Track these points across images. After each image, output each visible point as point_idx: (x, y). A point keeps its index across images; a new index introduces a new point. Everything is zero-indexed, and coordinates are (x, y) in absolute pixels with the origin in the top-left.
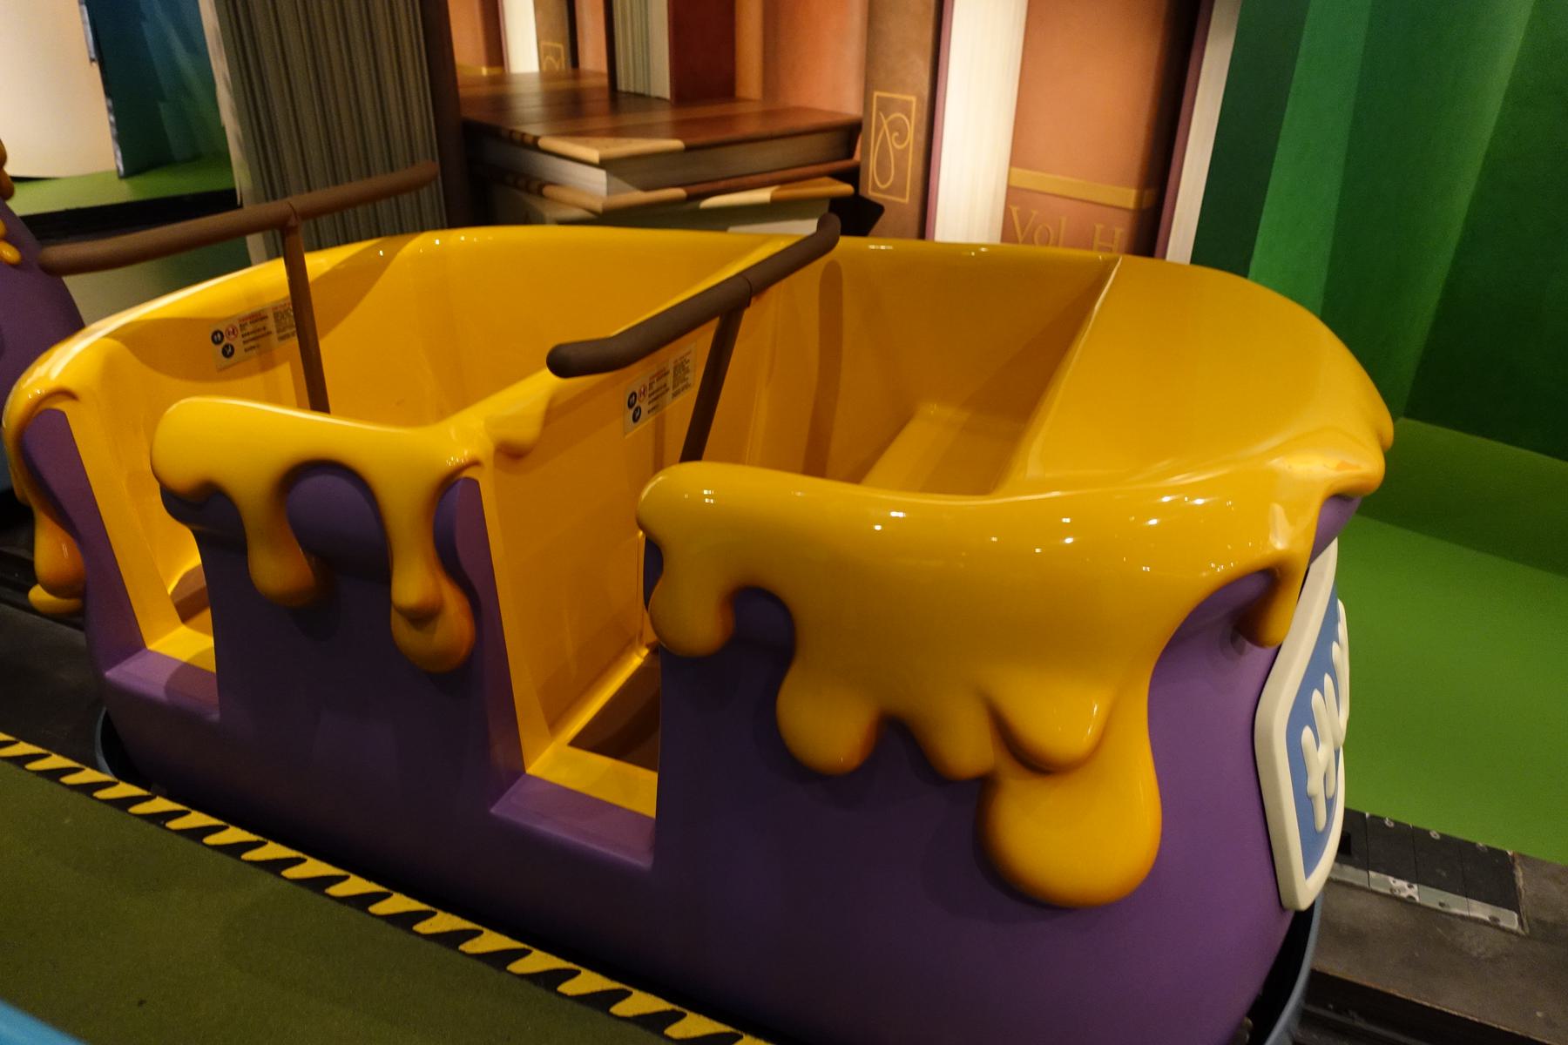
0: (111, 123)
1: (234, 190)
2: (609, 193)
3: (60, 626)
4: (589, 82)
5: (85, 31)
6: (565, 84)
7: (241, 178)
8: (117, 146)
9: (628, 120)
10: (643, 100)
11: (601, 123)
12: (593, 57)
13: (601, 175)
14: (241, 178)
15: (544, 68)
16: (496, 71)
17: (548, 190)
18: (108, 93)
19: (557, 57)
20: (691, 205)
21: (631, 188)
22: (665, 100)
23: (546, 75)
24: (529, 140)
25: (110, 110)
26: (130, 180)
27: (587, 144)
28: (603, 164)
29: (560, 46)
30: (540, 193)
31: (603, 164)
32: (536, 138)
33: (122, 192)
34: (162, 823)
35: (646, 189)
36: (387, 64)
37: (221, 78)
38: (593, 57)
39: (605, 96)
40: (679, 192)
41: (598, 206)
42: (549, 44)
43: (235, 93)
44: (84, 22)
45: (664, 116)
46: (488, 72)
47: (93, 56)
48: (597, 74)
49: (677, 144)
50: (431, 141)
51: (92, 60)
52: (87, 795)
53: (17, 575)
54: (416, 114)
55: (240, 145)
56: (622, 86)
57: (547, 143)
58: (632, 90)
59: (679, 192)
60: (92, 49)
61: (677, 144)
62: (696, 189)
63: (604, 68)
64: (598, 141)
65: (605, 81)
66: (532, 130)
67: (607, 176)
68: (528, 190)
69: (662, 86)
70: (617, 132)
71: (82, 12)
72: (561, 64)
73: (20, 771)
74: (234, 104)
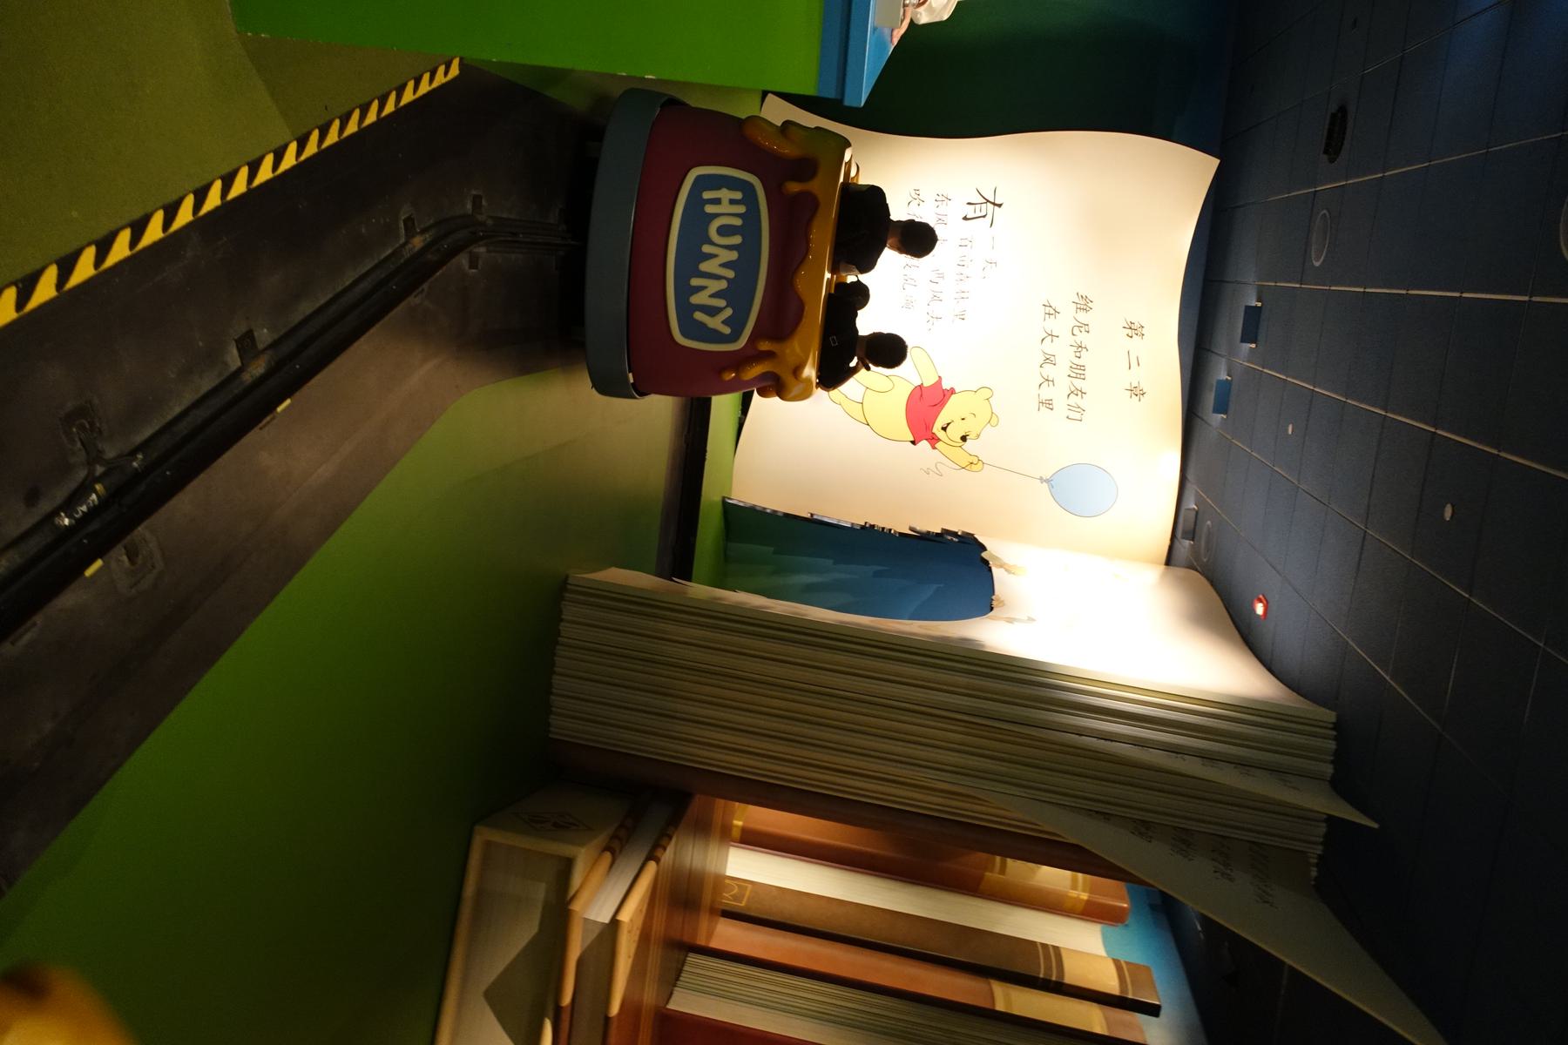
0: (765, 509)
1: (690, 580)
2: (586, 920)
3: (330, 296)
4: (704, 922)
5: (833, 519)
6: (707, 898)
7: (698, 590)
8: (748, 506)
9: (655, 955)
10: (671, 978)
11: (658, 927)
12: (728, 936)
13: (605, 918)
14: (698, 590)
15: (727, 881)
16: (736, 833)
17: (608, 856)
18: (787, 515)
19: (735, 898)
20: (551, 1011)
21: (586, 945)
22: (667, 1003)
23: (721, 881)
24: (658, 853)
25: (775, 511)
26: (721, 503)
27: (639, 910)
28: (614, 923)
29: (743, 904)
30: (607, 848)
31: (614, 923)
32: (657, 861)
33: (711, 492)
34: (20, 285)
35: (580, 963)
36: (732, 739)
37: (772, 605)
38: (728, 936)
39: (686, 938)
40: (567, 1000)
41: (576, 907)
42: (748, 893)
43: (755, 610)
44: (839, 521)
45: (649, 997)
46: (737, 826)
47: (815, 517)
48: (710, 935)
49: (615, 1009)
50: (646, 752)
51: (812, 515)
52: (97, 241)
53: (394, 287)
54: (819, 756)
55: (720, 599)
56: (692, 958)
57: (652, 867)
58: (686, 968)
59: (567, 1000)
60: (819, 518)
61: (615, 1009)
62: (566, 1017)
63: (714, 944)
64: (639, 922)
65: (701, 941)
66: (668, 856)
67: (603, 923)
68: (614, 837)
69: (685, 1002)
70: (645, 938)
71: (847, 522)
72: (728, 900)
73: (161, 204)
74: (748, 606)
